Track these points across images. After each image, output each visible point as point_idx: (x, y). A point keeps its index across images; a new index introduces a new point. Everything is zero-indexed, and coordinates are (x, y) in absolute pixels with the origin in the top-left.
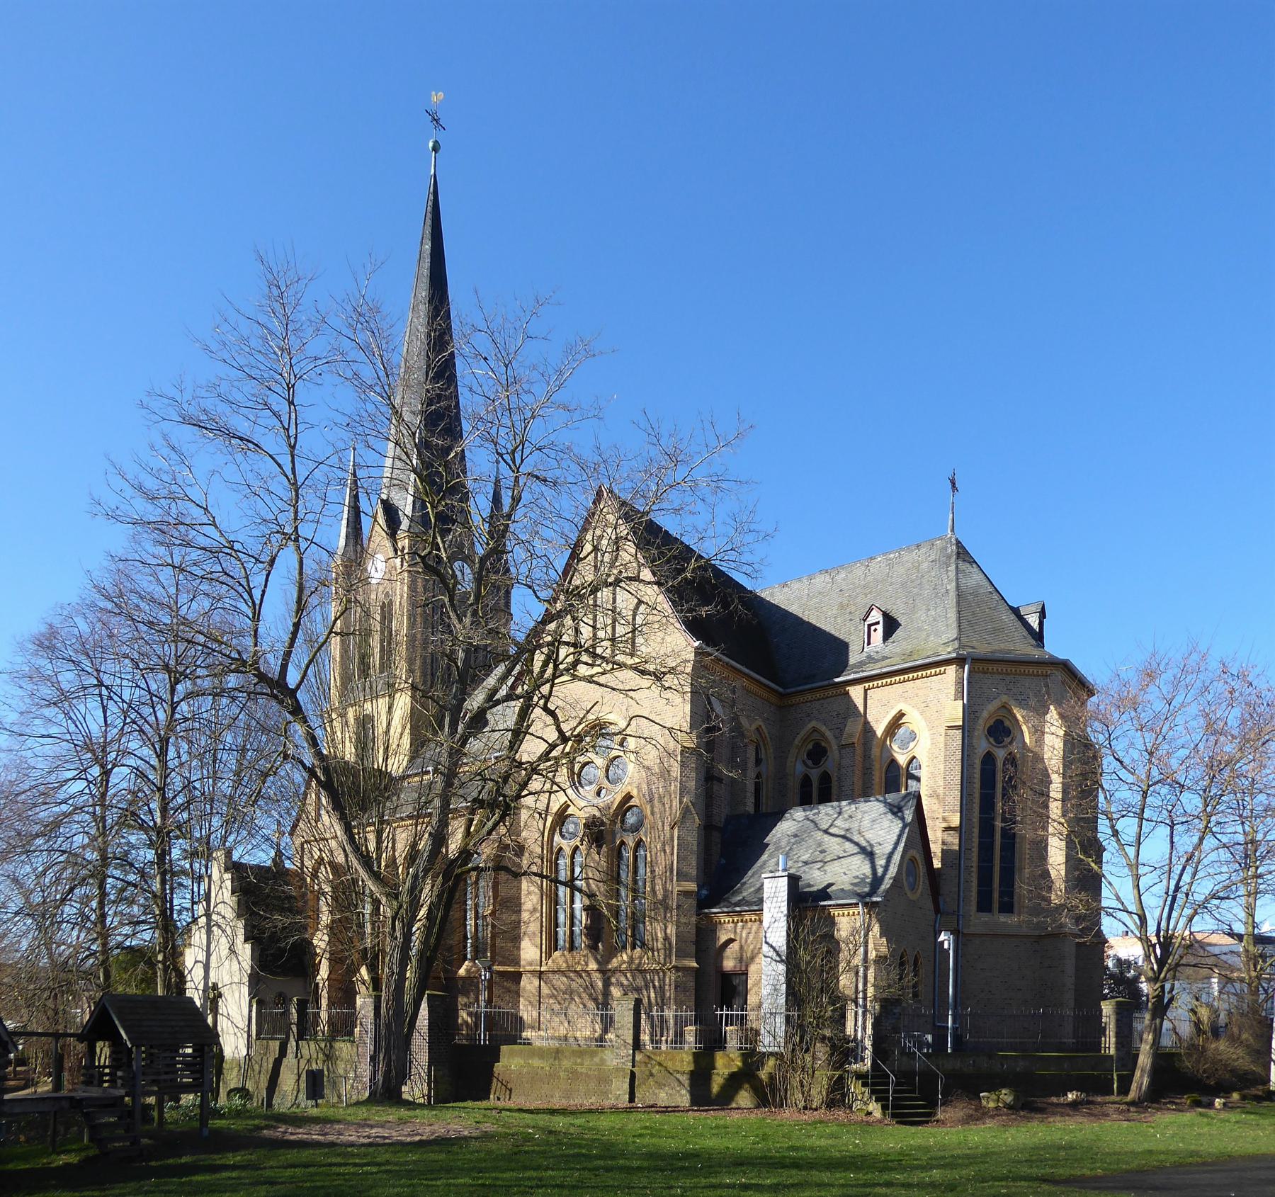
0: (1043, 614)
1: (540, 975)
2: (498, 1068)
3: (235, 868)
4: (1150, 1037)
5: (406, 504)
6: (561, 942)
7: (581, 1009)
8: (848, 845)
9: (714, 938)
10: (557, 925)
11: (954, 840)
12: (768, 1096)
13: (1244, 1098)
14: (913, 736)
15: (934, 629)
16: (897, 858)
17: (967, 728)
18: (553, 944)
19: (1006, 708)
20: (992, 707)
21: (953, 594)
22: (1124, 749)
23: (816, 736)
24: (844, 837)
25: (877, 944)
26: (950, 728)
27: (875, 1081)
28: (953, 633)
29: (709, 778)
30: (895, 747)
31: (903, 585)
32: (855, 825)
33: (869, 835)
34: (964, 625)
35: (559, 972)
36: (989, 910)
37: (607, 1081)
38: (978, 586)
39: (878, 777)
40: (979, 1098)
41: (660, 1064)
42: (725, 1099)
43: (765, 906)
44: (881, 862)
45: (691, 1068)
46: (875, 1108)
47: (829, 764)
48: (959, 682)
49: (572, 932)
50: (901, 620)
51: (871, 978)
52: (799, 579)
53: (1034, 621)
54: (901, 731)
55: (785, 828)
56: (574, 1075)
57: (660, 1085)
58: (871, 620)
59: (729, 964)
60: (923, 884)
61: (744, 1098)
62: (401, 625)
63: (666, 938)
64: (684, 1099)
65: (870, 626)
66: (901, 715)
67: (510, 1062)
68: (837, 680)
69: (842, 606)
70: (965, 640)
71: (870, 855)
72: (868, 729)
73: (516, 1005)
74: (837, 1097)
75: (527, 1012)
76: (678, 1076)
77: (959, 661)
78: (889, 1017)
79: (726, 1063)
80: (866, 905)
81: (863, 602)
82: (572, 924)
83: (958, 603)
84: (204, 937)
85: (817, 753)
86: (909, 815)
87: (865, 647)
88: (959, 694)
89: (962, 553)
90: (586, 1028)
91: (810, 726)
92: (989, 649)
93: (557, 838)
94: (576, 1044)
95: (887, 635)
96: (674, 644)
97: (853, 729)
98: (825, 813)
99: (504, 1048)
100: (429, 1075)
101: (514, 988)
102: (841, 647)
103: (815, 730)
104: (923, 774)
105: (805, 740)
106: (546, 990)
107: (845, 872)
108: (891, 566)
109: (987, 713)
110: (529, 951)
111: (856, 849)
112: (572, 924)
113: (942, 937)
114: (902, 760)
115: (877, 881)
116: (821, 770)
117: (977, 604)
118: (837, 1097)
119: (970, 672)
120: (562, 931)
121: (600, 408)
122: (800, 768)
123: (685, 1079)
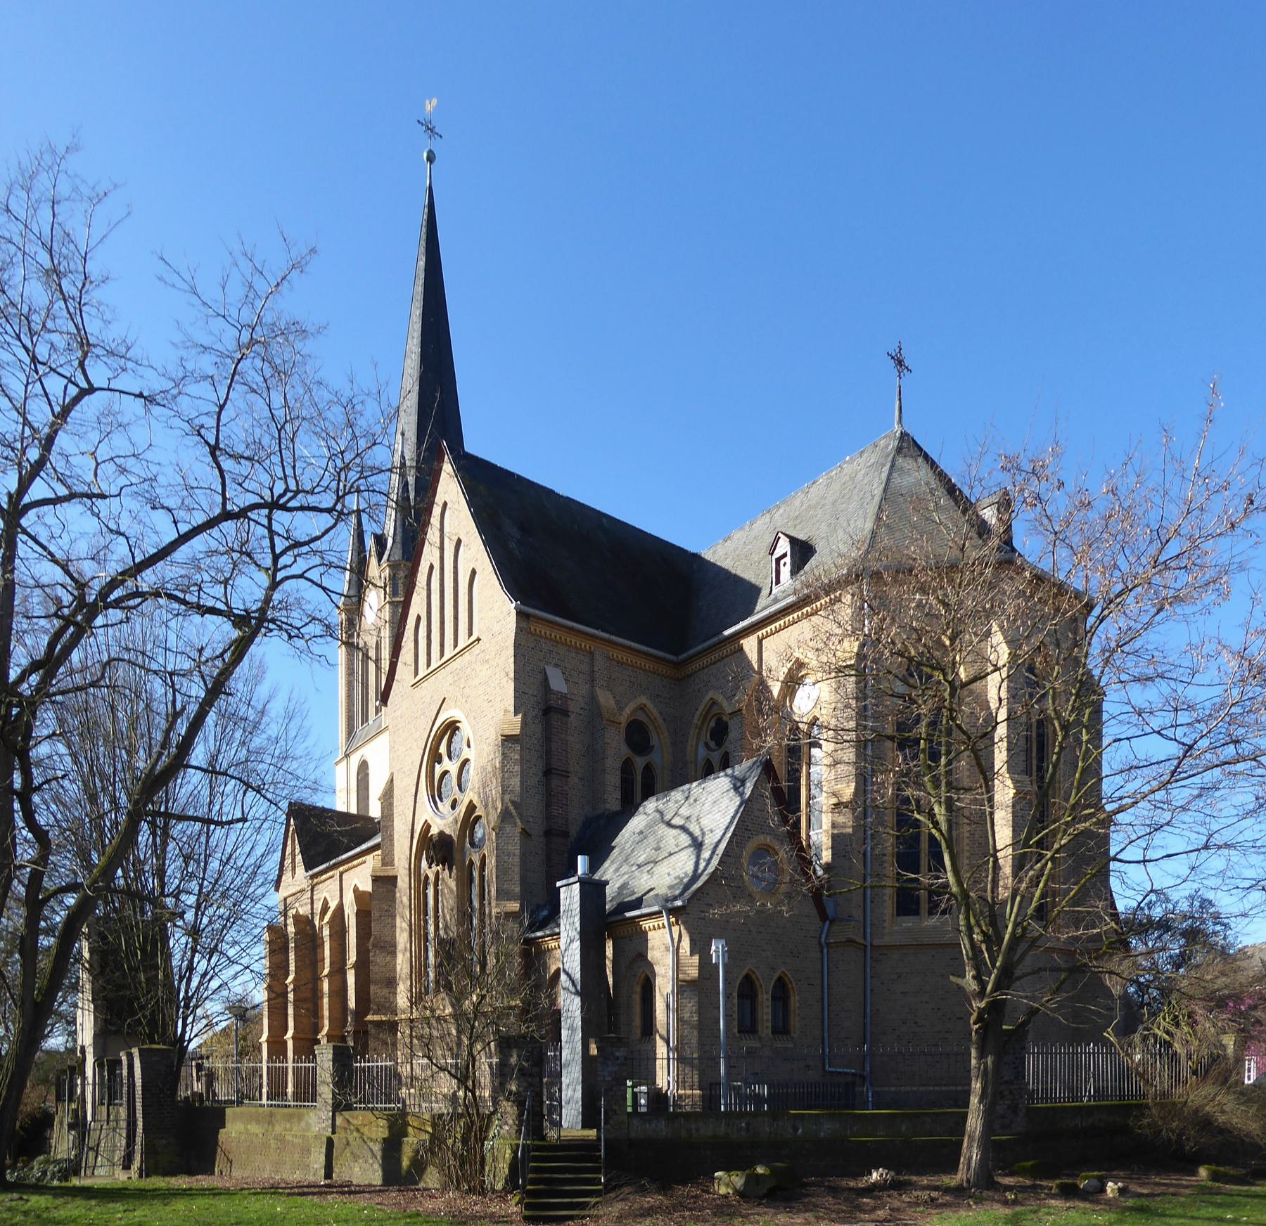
4: (979, 1085)
9: (545, 967)
11: (846, 819)
13: (1215, 1177)
16: (723, 846)
23: (715, 710)
36: (916, 913)
41: (358, 1130)
45: (386, 1135)
58: (778, 553)
64: (374, 1176)
65: (778, 560)
68: (727, 633)
71: (697, 845)
76: (371, 1144)
91: (708, 698)
95: (796, 569)
105: (705, 717)
115: (695, 877)
116: (722, 750)
123: (377, 1148)
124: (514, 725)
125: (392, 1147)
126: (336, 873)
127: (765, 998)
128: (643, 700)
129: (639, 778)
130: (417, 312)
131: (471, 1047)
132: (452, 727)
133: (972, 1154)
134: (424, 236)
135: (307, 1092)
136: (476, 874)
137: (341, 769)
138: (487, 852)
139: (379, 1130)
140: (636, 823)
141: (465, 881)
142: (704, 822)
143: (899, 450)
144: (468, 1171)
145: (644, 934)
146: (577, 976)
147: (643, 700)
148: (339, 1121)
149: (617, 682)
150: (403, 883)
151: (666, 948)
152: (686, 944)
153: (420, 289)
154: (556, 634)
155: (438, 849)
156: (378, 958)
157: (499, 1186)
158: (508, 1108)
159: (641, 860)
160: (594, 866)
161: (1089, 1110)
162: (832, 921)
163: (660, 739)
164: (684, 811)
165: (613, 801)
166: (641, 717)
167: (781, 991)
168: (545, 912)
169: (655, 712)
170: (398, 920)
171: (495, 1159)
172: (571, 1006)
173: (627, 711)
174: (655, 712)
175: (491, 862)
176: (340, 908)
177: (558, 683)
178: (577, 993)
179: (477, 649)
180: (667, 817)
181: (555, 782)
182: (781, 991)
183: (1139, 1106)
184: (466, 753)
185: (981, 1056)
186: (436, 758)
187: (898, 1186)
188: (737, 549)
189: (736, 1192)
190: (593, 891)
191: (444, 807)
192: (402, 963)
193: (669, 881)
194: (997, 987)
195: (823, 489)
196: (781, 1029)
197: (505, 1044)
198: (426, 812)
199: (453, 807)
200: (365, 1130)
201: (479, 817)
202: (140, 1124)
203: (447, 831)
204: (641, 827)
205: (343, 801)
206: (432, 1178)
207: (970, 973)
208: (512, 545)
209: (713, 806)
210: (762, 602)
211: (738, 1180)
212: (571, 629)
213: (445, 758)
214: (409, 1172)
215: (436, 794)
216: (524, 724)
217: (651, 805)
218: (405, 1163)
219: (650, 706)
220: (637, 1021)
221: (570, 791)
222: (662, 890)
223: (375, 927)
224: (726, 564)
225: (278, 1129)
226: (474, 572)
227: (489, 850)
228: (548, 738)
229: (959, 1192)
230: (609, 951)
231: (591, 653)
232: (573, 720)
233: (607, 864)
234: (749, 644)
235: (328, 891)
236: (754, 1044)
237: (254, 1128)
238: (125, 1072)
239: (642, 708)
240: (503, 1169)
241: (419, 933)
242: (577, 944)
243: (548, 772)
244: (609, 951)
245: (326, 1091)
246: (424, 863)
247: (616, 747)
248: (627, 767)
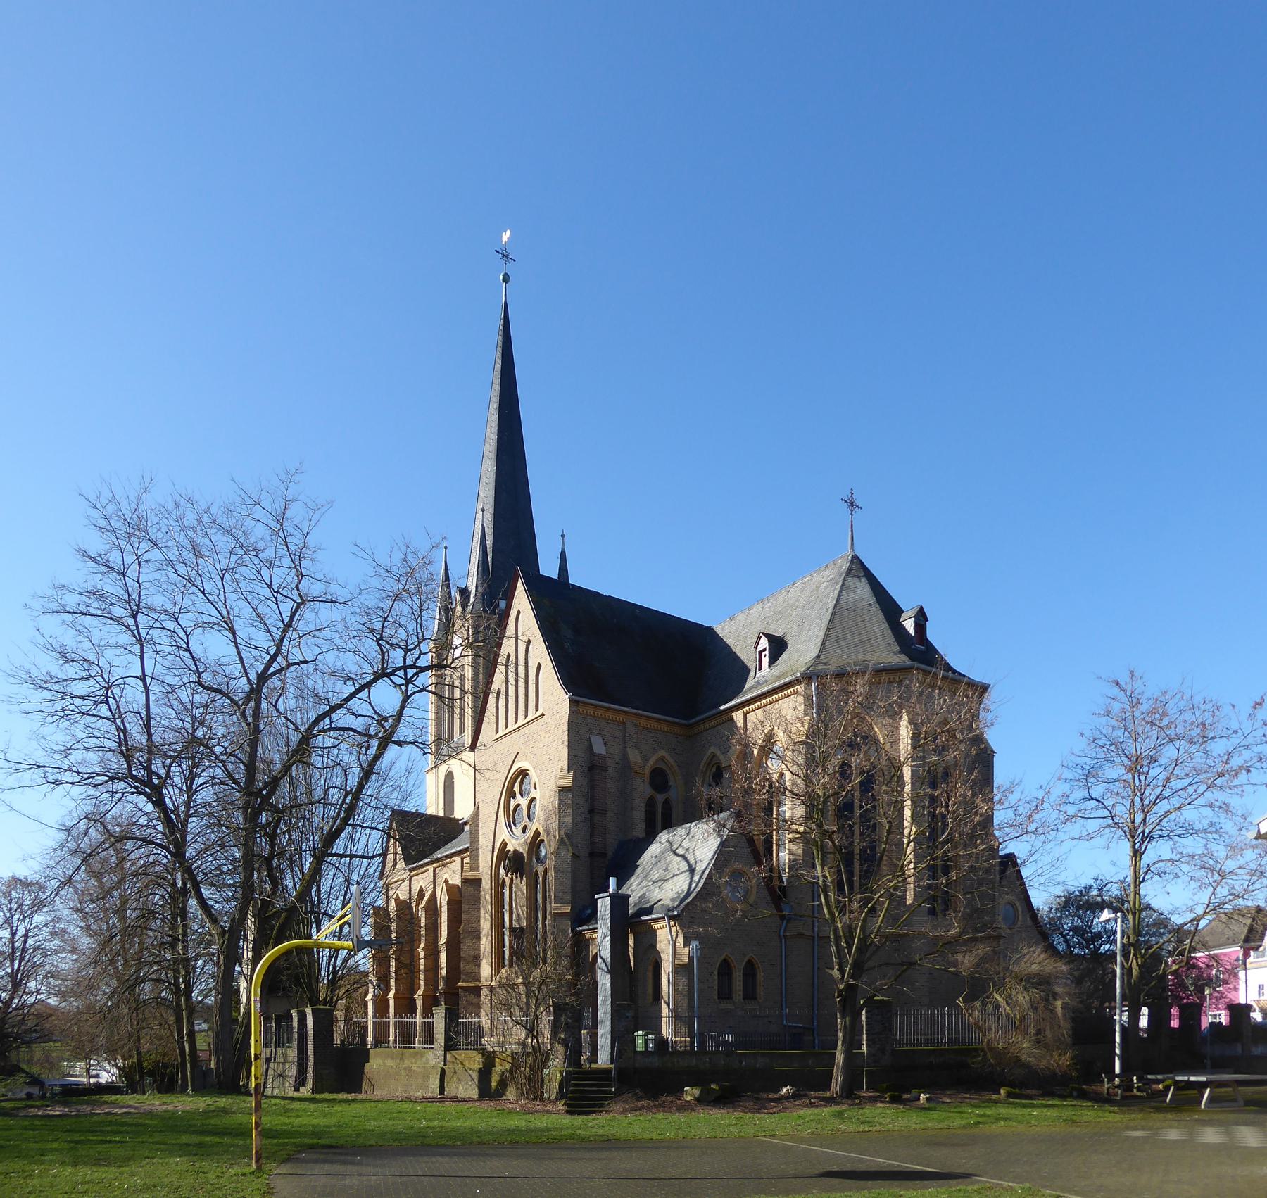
6: (506, 963)
13: (1009, 1095)
16: (707, 873)
38: (861, 599)
52: (743, 612)
53: (909, 626)
58: (760, 647)
64: (474, 1093)
65: (761, 653)
71: (692, 870)
95: (773, 660)
101: (475, 1001)
102: (741, 672)
109: (840, 729)
115: (688, 894)
119: (817, 688)
123: (475, 1075)
124: (568, 779)
125: (485, 1074)
126: (431, 869)
127: (738, 977)
128: (663, 753)
129: (660, 810)
130: (495, 406)
131: (537, 1006)
132: (523, 773)
133: (838, 1078)
134: (500, 344)
135: (429, 1039)
136: (540, 880)
137: (430, 778)
138: (550, 866)
139: (476, 1061)
140: (654, 849)
141: (532, 887)
142: (697, 853)
143: (849, 571)
144: (534, 1089)
145: (655, 931)
146: (609, 960)
147: (663, 753)
148: (449, 1056)
149: (642, 742)
150: (486, 885)
151: (670, 943)
153: (497, 387)
155: (513, 862)
156: (467, 942)
157: (553, 1097)
158: (559, 1048)
160: (620, 885)
161: (942, 1052)
162: (789, 920)
163: (676, 781)
164: (686, 844)
165: (639, 830)
166: (663, 766)
167: (750, 971)
168: (585, 915)
169: (671, 761)
170: (482, 912)
171: (550, 1080)
172: (604, 981)
173: (651, 762)
174: (671, 761)
175: (551, 875)
176: (434, 895)
177: (599, 748)
178: (608, 972)
179: (541, 721)
181: (597, 818)
182: (750, 971)
183: (976, 1050)
184: (533, 793)
185: (843, 1017)
186: (511, 794)
187: (795, 1096)
188: (739, 633)
189: (696, 1099)
190: (619, 902)
191: (517, 830)
192: (485, 944)
193: (672, 895)
194: (852, 976)
195: (797, 592)
196: (750, 995)
197: (559, 1009)
198: (503, 834)
199: (524, 831)
200: (466, 1063)
201: (542, 841)
202: (311, 1059)
203: (520, 849)
204: (657, 853)
205: (432, 805)
206: (511, 1094)
208: (567, 645)
209: (699, 843)
210: (750, 683)
211: (697, 1091)
212: (610, 708)
213: (518, 795)
214: (497, 1089)
215: (511, 820)
216: (575, 777)
217: (664, 836)
218: (494, 1084)
219: (668, 758)
220: (650, 991)
221: (604, 829)
222: (666, 902)
223: (465, 918)
224: (730, 641)
225: (407, 1063)
226: (539, 666)
227: (550, 864)
228: (592, 787)
229: (830, 1101)
230: (631, 942)
231: (624, 723)
232: (610, 772)
233: (633, 879)
234: (738, 716)
235: (422, 881)
236: (730, 1006)
237: (389, 1062)
238: (295, 1024)
239: (662, 759)
240: (555, 1086)
241: (498, 923)
242: (609, 938)
243: (592, 811)
244: (631, 942)
245: (440, 1036)
246: (502, 871)
247: (642, 789)
248: (650, 803)
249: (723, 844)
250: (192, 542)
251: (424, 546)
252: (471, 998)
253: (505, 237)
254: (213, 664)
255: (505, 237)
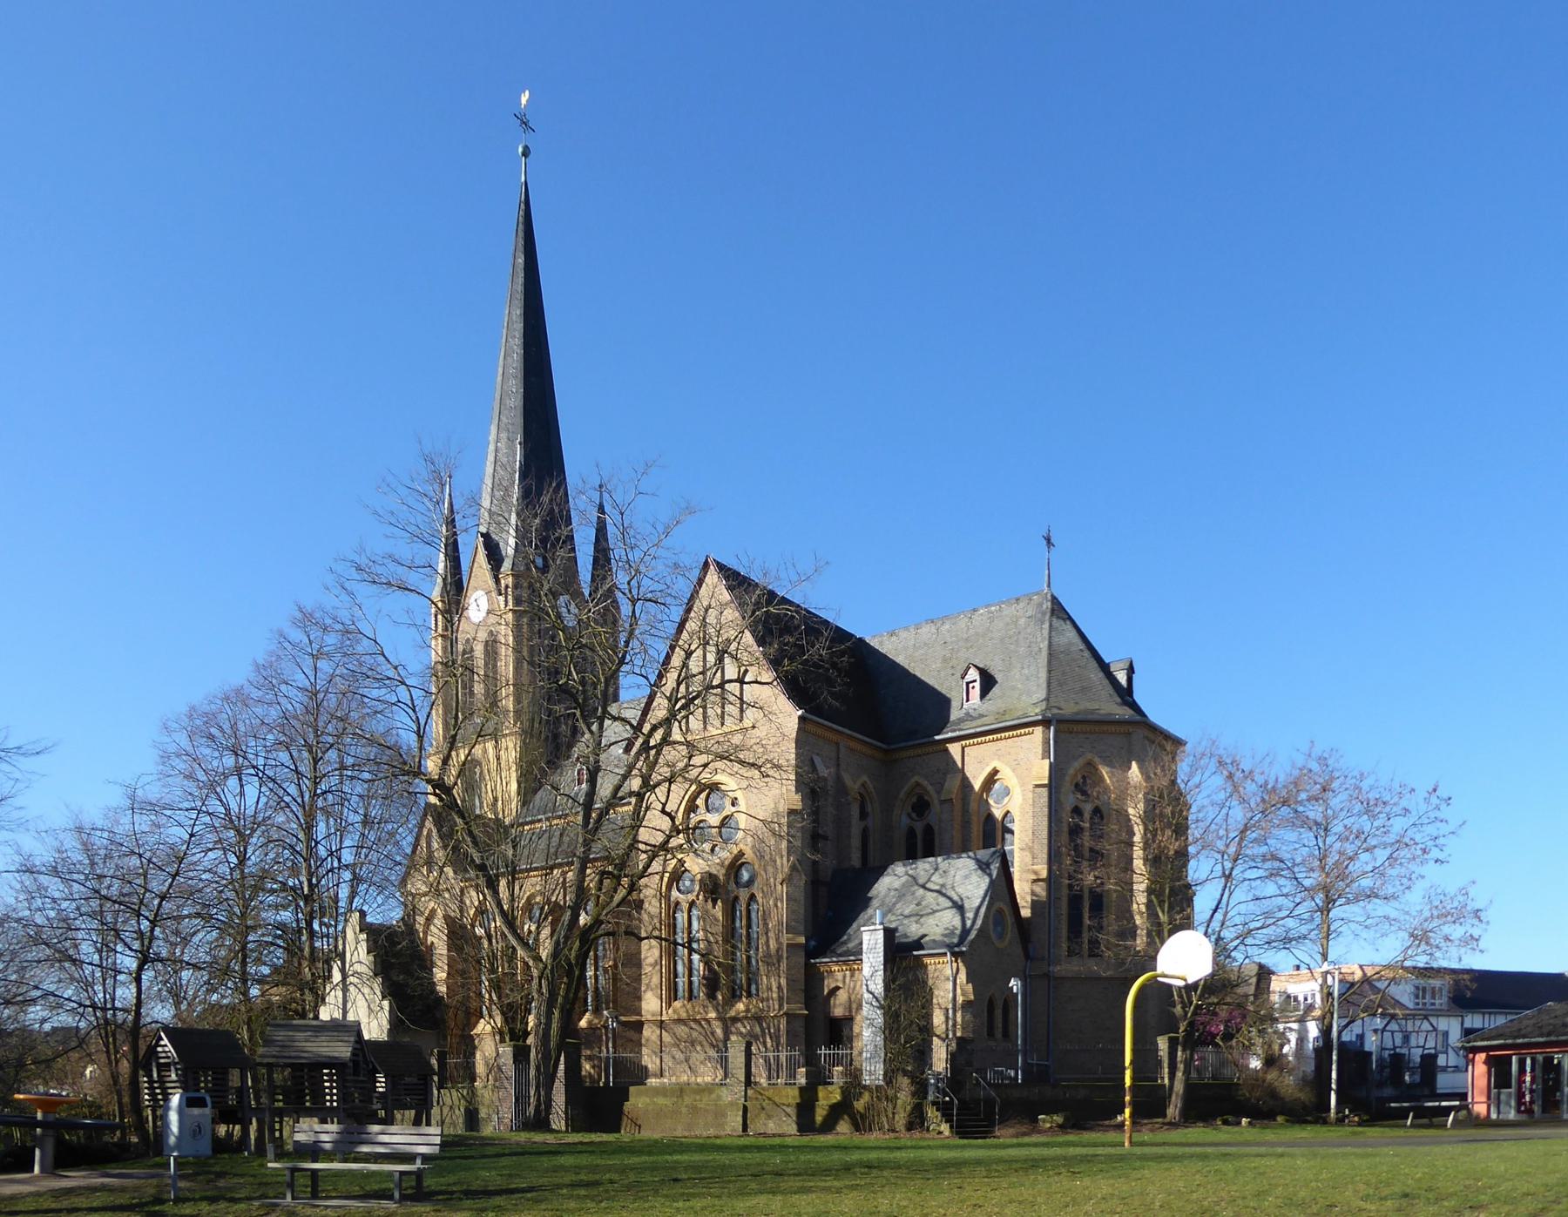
0: (1131, 670)
1: (661, 1025)
2: (627, 1106)
3: (365, 927)
5: (509, 545)
6: (680, 993)
7: (702, 1056)
8: (942, 899)
10: (676, 976)
11: (1041, 890)
12: (861, 1123)
14: (1007, 791)
15: (1026, 688)
16: (983, 910)
17: (1054, 786)
18: (673, 994)
19: (1090, 764)
20: (1077, 764)
21: (1045, 653)
22: (1206, 797)
24: (938, 892)
25: (965, 990)
26: (1037, 786)
27: (945, 1111)
28: (1042, 694)
29: (815, 838)
30: (991, 802)
31: (1002, 640)
32: (949, 882)
33: (960, 890)
34: (1054, 685)
35: (679, 1021)
37: (724, 1115)
38: (1070, 644)
39: (976, 830)
40: (1037, 1121)
42: (829, 1126)
43: (864, 957)
44: (970, 915)
46: (945, 1128)
47: (931, 818)
48: (1046, 742)
49: (691, 983)
50: (998, 677)
51: (959, 1020)
52: (906, 628)
53: (1122, 678)
54: (997, 785)
55: (890, 882)
56: (694, 1110)
57: (769, 1117)
59: (838, 1012)
60: (1011, 932)
61: (844, 1127)
62: (507, 666)
63: (780, 987)
64: (791, 1127)
66: (995, 772)
67: (637, 1101)
69: (945, 660)
70: (1053, 702)
71: (959, 907)
72: (966, 784)
73: (640, 1052)
74: (917, 1121)
75: (649, 1060)
77: (1045, 723)
78: (962, 1053)
79: (829, 1096)
80: (954, 954)
81: (964, 656)
82: (690, 975)
83: (1049, 662)
84: (340, 994)
85: (921, 806)
86: (995, 868)
87: (967, 703)
88: (1046, 754)
89: (1058, 610)
90: (708, 1074)
92: (1075, 709)
93: (675, 893)
94: (690, 1074)
95: (985, 692)
96: (774, 718)
97: (953, 784)
98: (923, 866)
99: (632, 1089)
100: (566, 1113)
102: (943, 703)
103: (918, 784)
104: (1015, 827)
106: (667, 1037)
107: (940, 924)
108: (991, 620)
110: (651, 1004)
111: (946, 903)
112: (690, 975)
113: (1012, 982)
114: (998, 813)
115: (965, 932)
117: (1076, 656)
118: (917, 1121)
120: (682, 982)
121: (704, 494)
122: (905, 821)
123: (792, 1111)
145: (926, 966)
151: (948, 984)
152: (962, 977)
154: (819, 731)
159: (907, 912)
180: (921, 881)
203: (714, 871)
207: (1179, 1007)
249: (992, 882)
250: (709, 607)
251: (1300, 762)
252: (631, 1034)
253: (524, 99)
254: (1419, 870)
255: (524, 99)
